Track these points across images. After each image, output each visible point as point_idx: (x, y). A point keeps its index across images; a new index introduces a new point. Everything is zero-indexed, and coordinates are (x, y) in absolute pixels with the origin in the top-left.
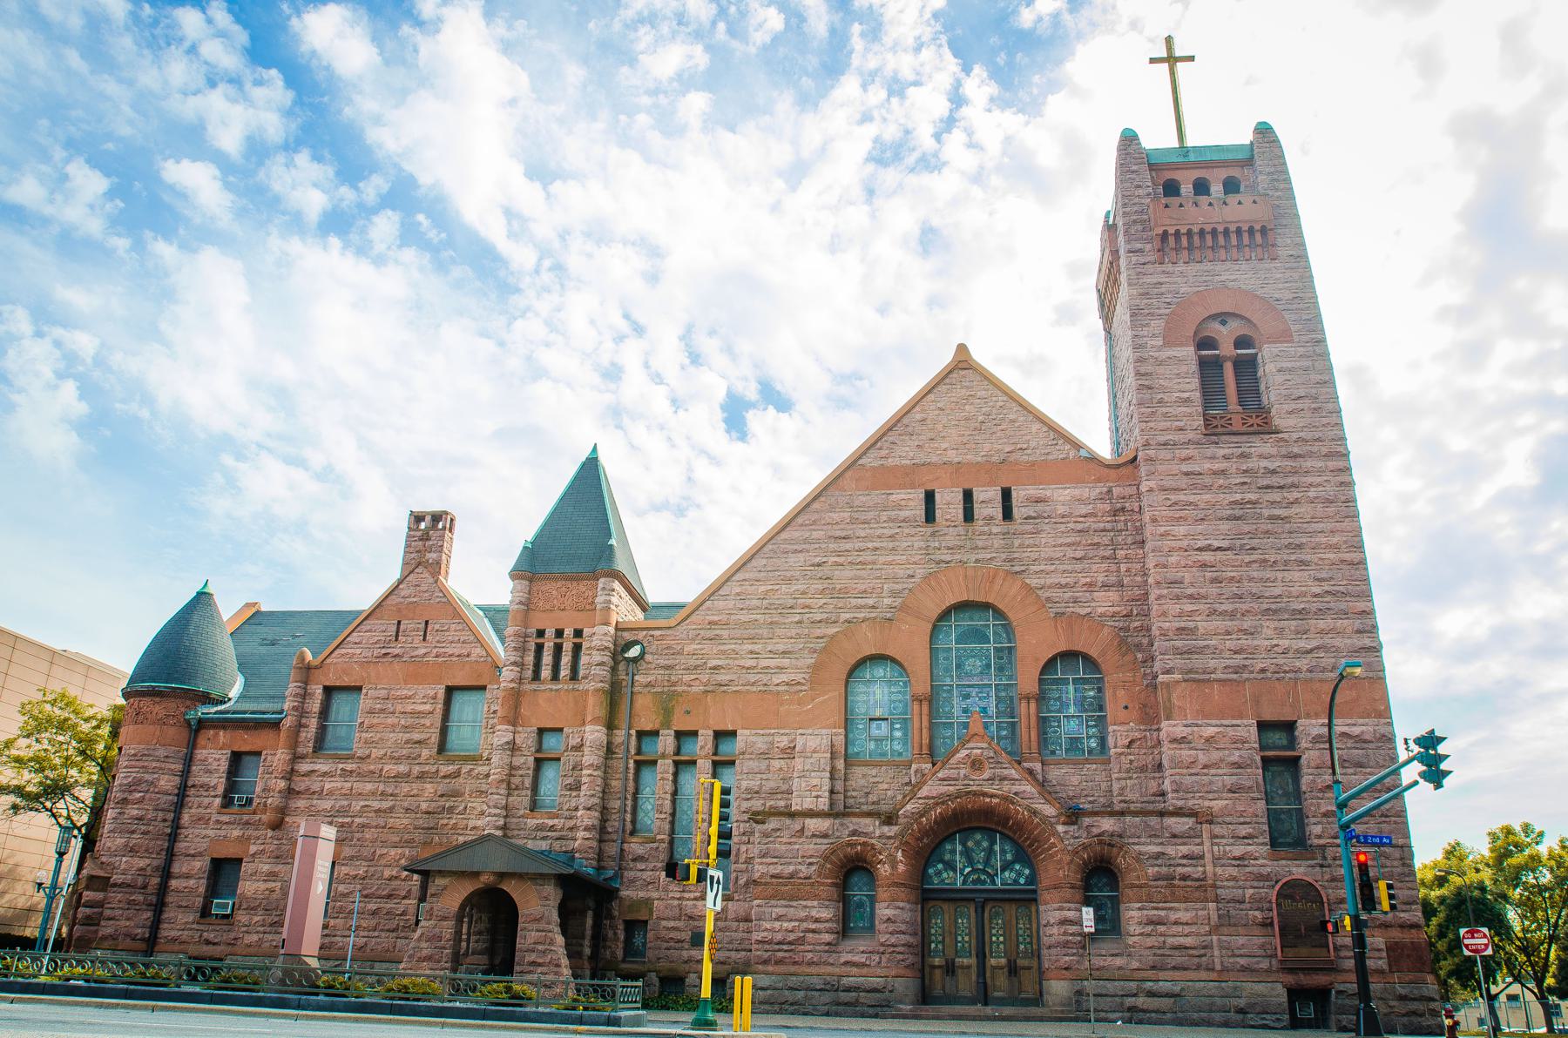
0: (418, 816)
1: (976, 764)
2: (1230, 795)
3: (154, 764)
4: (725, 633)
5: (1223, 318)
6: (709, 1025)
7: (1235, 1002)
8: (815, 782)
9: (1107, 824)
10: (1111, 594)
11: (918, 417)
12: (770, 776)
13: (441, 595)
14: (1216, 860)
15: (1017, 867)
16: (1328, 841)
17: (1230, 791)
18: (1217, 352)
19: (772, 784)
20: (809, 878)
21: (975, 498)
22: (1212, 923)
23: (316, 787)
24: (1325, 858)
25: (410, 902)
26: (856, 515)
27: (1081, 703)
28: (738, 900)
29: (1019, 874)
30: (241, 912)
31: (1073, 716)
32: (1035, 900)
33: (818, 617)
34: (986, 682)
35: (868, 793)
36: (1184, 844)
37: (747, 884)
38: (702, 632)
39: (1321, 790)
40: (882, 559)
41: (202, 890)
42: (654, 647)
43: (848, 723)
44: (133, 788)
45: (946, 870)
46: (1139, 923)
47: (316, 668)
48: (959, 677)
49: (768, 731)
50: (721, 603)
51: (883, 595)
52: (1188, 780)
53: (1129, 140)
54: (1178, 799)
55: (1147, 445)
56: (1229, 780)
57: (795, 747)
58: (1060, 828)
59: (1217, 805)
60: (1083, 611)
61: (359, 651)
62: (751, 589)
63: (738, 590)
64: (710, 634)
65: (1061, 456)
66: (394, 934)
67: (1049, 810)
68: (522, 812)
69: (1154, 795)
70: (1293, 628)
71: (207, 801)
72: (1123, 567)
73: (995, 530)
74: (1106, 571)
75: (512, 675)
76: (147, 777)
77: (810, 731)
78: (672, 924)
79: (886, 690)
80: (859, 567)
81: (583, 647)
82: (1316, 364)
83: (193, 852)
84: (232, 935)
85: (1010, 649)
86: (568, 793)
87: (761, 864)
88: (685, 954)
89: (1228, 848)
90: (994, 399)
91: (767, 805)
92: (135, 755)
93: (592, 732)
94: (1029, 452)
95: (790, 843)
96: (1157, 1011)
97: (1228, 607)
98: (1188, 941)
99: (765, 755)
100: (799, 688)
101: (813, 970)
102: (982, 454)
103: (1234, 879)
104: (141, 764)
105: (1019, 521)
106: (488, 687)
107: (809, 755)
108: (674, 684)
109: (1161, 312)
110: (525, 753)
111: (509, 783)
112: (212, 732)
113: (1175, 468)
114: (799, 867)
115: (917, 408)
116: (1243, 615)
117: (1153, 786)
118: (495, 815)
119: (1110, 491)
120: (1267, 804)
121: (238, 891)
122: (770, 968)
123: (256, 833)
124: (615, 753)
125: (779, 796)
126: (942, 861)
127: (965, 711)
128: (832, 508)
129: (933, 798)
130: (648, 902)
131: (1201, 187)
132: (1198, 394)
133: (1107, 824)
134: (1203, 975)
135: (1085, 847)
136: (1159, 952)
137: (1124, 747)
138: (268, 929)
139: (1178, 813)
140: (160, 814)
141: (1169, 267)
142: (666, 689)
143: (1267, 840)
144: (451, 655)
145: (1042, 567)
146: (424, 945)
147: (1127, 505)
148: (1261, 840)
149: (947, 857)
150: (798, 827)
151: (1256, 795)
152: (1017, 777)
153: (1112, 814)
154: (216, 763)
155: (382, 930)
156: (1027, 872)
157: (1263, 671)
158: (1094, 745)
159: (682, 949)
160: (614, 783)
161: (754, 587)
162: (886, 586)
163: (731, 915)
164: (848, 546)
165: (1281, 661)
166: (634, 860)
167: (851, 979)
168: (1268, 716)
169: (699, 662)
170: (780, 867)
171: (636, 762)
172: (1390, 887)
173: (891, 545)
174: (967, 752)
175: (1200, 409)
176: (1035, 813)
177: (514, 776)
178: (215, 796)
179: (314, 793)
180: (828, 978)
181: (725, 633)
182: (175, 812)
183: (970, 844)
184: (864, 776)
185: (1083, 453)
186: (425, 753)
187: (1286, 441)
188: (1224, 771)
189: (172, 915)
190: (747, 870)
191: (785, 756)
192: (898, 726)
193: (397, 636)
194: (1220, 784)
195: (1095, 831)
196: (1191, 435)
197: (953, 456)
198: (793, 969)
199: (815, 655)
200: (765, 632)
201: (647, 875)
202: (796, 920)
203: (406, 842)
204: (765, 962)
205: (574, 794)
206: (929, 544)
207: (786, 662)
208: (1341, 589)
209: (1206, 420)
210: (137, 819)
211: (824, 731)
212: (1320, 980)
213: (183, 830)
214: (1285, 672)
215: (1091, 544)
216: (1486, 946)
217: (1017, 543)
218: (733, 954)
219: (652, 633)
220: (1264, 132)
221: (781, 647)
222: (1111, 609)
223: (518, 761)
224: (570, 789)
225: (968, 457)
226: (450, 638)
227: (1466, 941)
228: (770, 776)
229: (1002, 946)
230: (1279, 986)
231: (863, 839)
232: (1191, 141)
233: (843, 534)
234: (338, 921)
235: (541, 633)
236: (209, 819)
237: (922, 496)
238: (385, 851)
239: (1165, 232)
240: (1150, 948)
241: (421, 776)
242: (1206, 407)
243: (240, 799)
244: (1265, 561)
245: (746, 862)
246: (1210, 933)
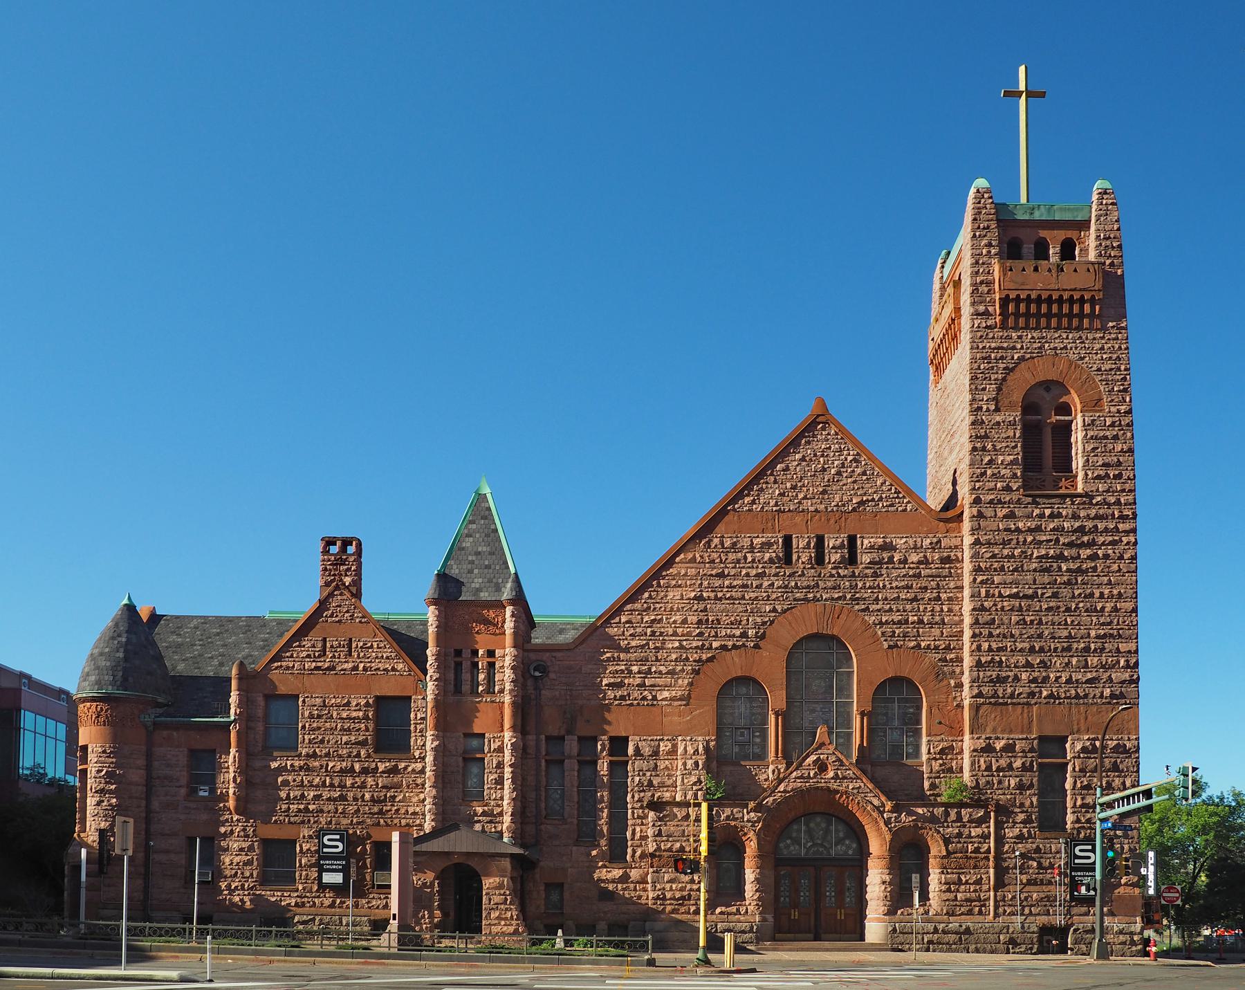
1: (822, 767)
15: (847, 842)
29: (849, 847)
45: (793, 844)
91: (656, 796)
126: (791, 838)
147: (952, 554)
149: (794, 835)
171: (546, 761)
183: (812, 825)
192: (758, 734)
216: (1178, 898)
219: (554, 654)
229: (833, 899)
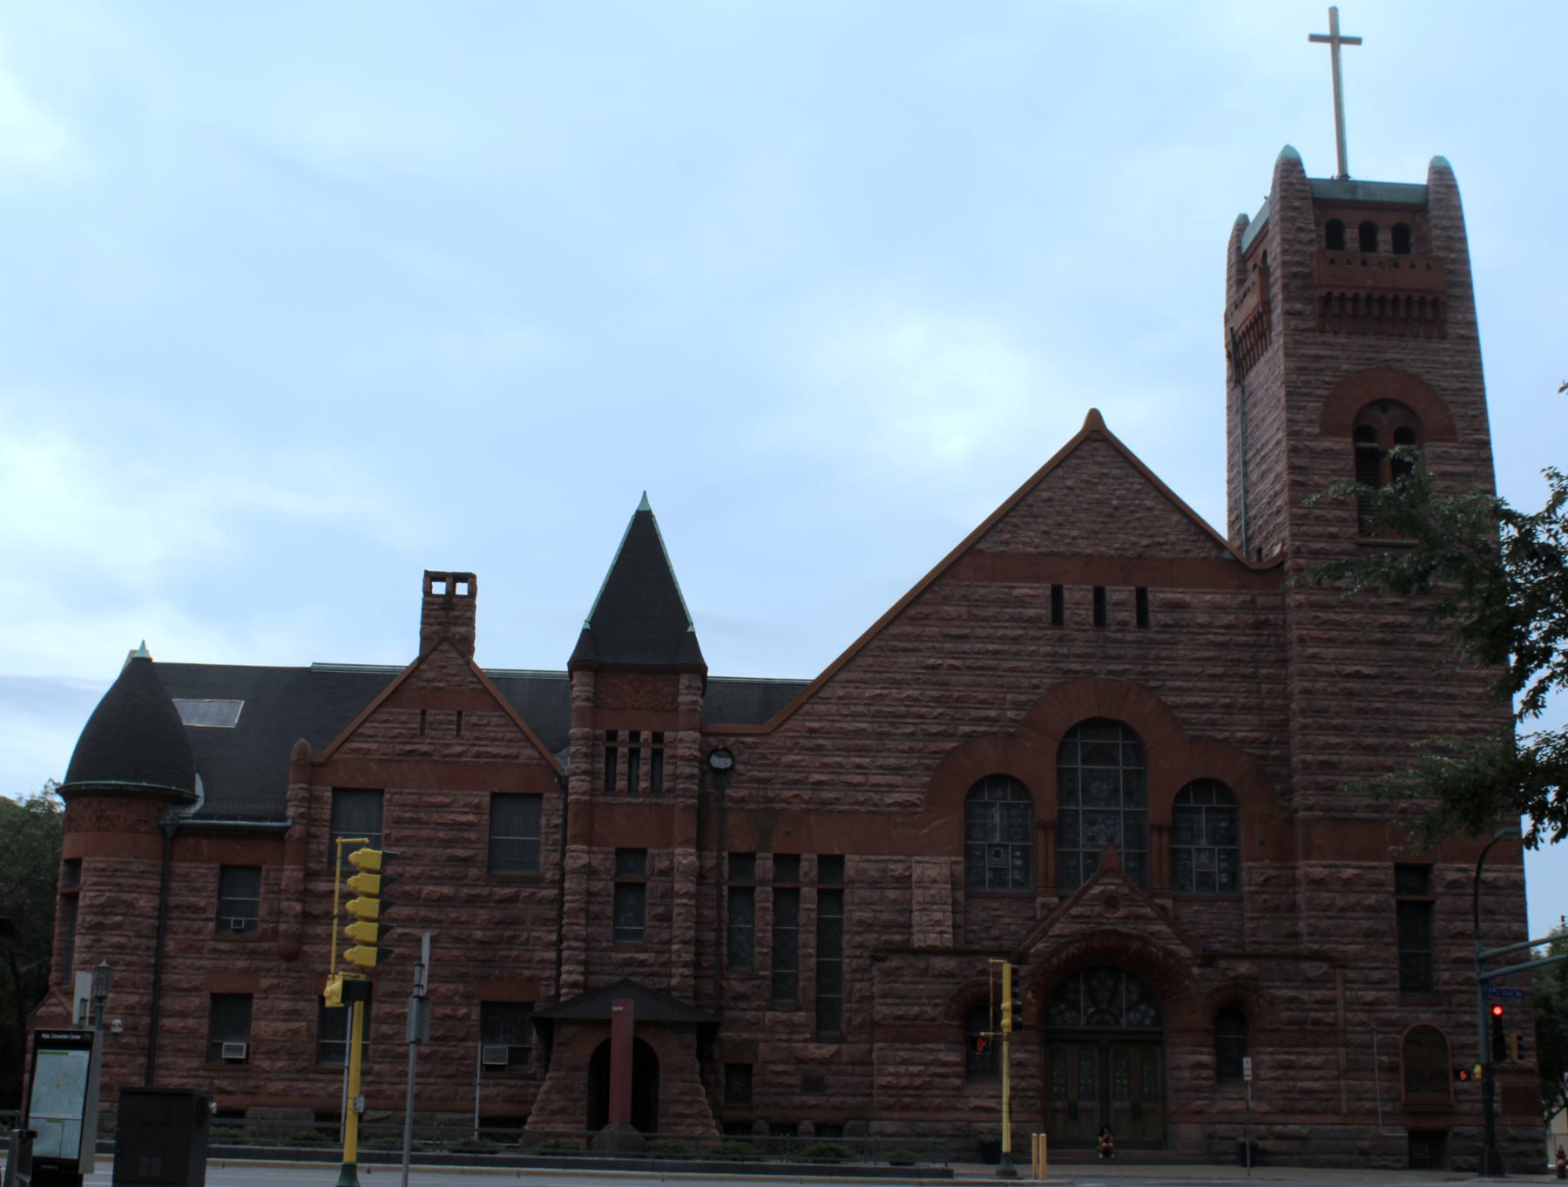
1: (1111, 901)
5: (1383, 404)
6: (1013, 1174)
8: (938, 916)
9: (1244, 968)
10: (1250, 717)
11: (1045, 495)
13: (475, 680)
15: (1143, 1007)
16: (1456, 987)
18: (1375, 445)
21: (1107, 599)
24: (1450, 1004)
26: (975, 611)
31: (1205, 849)
33: (934, 729)
34: (1113, 808)
36: (1318, 988)
41: (205, 1030)
42: (746, 756)
44: (108, 910)
46: (1271, 1068)
47: (321, 765)
48: (1085, 802)
51: (1007, 706)
52: (1325, 923)
53: (1289, 167)
55: (1297, 552)
58: (1196, 970)
60: (1220, 736)
62: (856, 692)
63: (841, 693)
64: (809, 743)
65: (1202, 555)
67: (1185, 951)
68: (604, 944)
69: (1287, 936)
71: (198, 925)
73: (1130, 637)
74: (1245, 692)
75: (585, 786)
77: (927, 859)
78: (780, 1068)
81: (665, 755)
82: (1479, 469)
85: (1140, 772)
86: (658, 924)
88: (797, 1100)
92: (103, 870)
94: (1167, 547)
97: (1371, 741)
98: (1316, 1085)
100: (913, 809)
101: (942, 1116)
102: (1117, 546)
103: (1362, 1023)
105: (1155, 629)
107: (928, 885)
110: (603, 877)
111: (587, 911)
112: (191, 841)
114: (925, 1008)
115: (1043, 485)
119: (1253, 601)
122: (895, 1115)
123: (266, 965)
128: (946, 600)
133: (1244, 968)
136: (1289, 1096)
137: (1258, 884)
138: (296, 1076)
139: (1314, 956)
141: (1330, 338)
142: (762, 806)
143: (1397, 986)
146: (555, 1097)
148: (1391, 986)
150: (922, 965)
151: (1388, 940)
155: (440, 1076)
156: (1152, 1012)
158: (1224, 880)
164: (966, 647)
167: (981, 1124)
170: (904, 1008)
172: (1519, 1038)
174: (1102, 888)
175: (1355, 514)
176: (1171, 954)
178: (207, 920)
180: (958, 1124)
185: (1226, 555)
186: (473, 872)
189: (170, 1059)
191: (900, 885)
192: (1018, 854)
193: (422, 729)
195: (1231, 974)
196: (1345, 545)
197: (1084, 547)
199: (931, 773)
201: (751, 1015)
202: (922, 1064)
205: (665, 925)
207: (897, 779)
211: (943, 859)
213: (169, 961)
219: (742, 739)
220: (1442, 174)
221: (892, 762)
223: (598, 886)
229: (1125, 1089)
234: (383, 1066)
235: (612, 735)
237: (1048, 592)
244: (1412, 692)
246: (1337, 1078)
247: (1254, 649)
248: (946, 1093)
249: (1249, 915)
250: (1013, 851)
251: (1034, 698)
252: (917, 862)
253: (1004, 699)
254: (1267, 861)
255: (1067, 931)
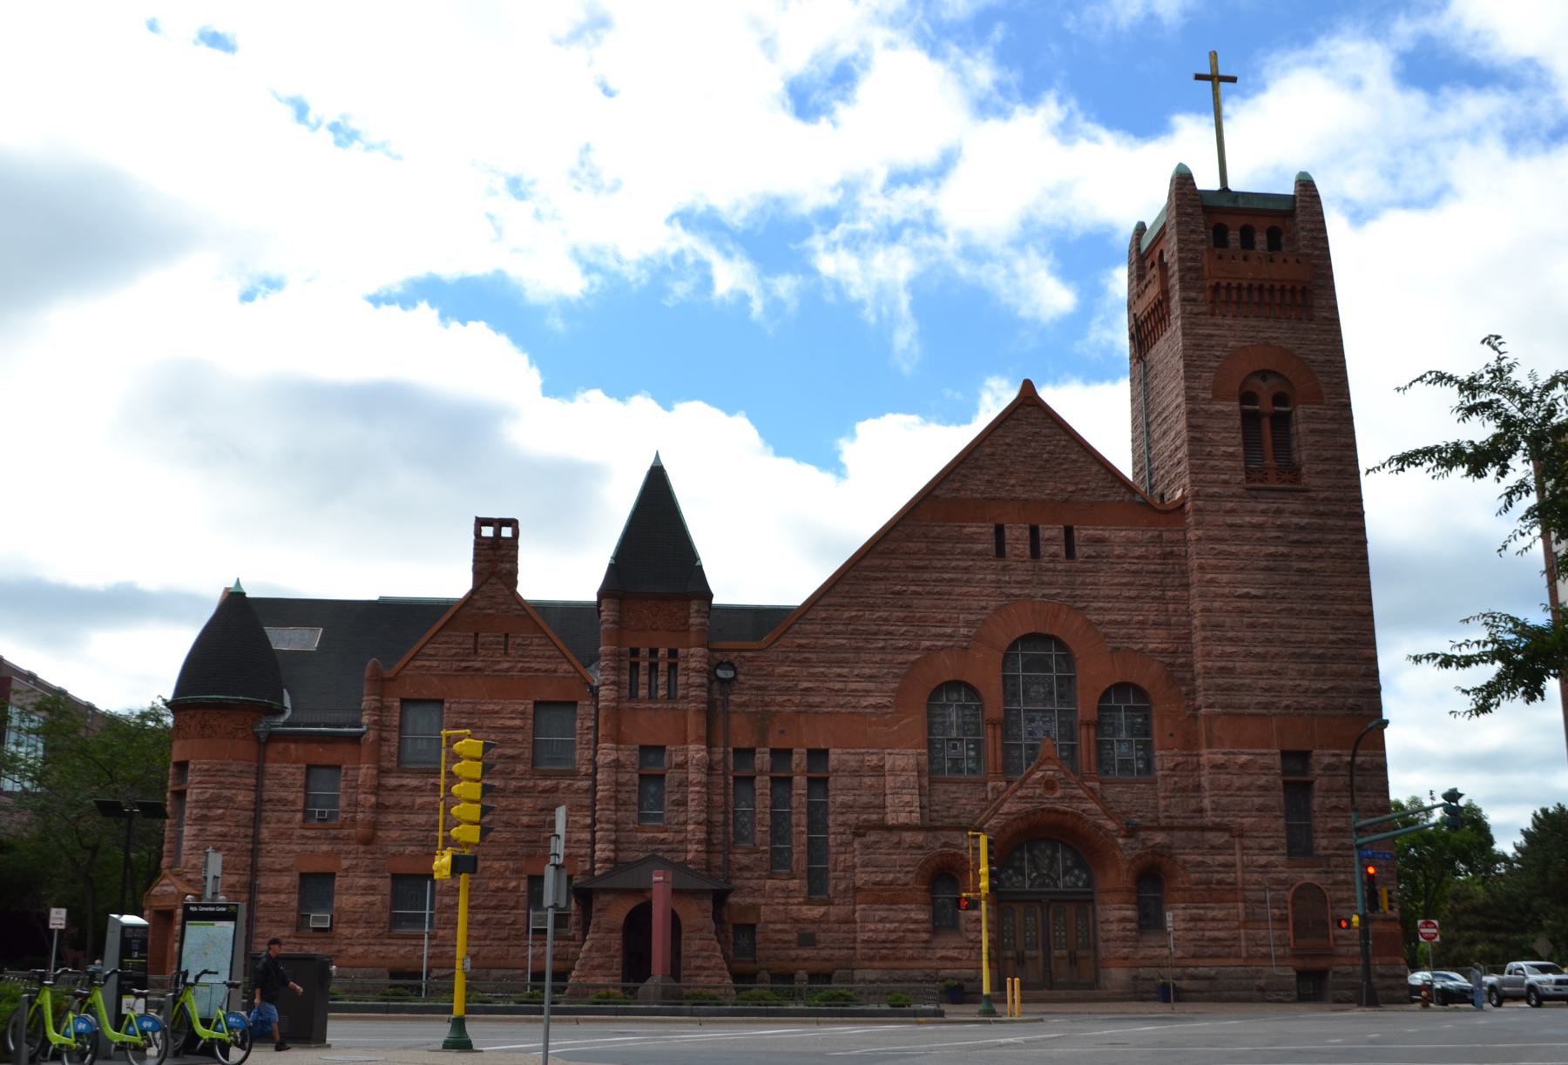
0: (519, 829)
1: (1050, 785)
2: (1258, 813)
3: (231, 780)
4: (813, 656)
5: (1264, 374)
7: (1257, 982)
8: (907, 798)
9: (1160, 838)
10: (1160, 631)
11: (988, 450)
12: (862, 792)
13: (519, 607)
14: (1245, 866)
17: (1258, 810)
18: (1257, 407)
19: (865, 799)
20: (906, 884)
22: (1241, 919)
23: (407, 801)
24: (1329, 866)
25: (520, 911)
27: (1132, 730)
28: (839, 904)
30: (340, 925)
32: (1092, 901)
35: (949, 808)
36: (1220, 854)
37: (846, 890)
38: (791, 654)
39: (1329, 810)
40: (958, 590)
41: (295, 904)
42: (746, 668)
43: (930, 744)
44: (212, 804)
46: (1183, 920)
49: (859, 750)
50: (808, 627)
52: (1225, 801)
54: (1217, 816)
56: (1258, 801)
57: (884, 765)
58: (1120, 841)
59: (1248, 821)
61: (435, 664)
63: (824, 615)
64: (798, 657)
66: (506, 943)
68: (631, 826)
69: (1194, 811)
70: (1312, 670)
71: (286, 816)
72: (1171, 607)
73: (1060, 567)
75: (613, 695)
76: (226, 793)
77: (896, 751)
78: (779, 926)
79: (960, 713)
80: (936, 597)
83: (279, 867)
84: (336, 948)
87: (863, 872)
88: (793, 953)
89: (1255, 858)
90: (1058, 438)
93: (698, 751)
94: (1089, 492)
95: (889, 854)
96: (1198, 991)
98: (1221, 934)
99: (855, 773)
100: (885, 710)
101: (914, 964)
104: (217, 779)
105: (1081, 559)
106: (580, 702)
108: (767, 704)
109: (1211, 364)
112: (281, 745)
113: (1220, 519)
114: (898, 875)
115: (987, 443)
116: (1273, 658)
117: (1193, 804)
118: (607, 830)
119: (1160, 536)
120: (1287, 820)
121: (335, 905)
122: (876, 964)
123: (345, 848)
124: (715, 770)
125: (872, 810)
127: (1031, 733)
129: (1013, 814)
130: (755, 908)
131: (1247, 236)
132: (1241, 449)
133: (1160, 838)
134: (1232, 961)
135: (1139, 857)
136: (1199, 943)
138: (372, 941)
139: (1217, 828)
140: (242, 830)
141: (1219, 320)
142: (760, 709)
143: (1285, 851)
144: (537, 670)
145: (1100, 604)
146: (594, 954)
148: (1281, 851)
150: (895, 839)
151: (1278, 814)
152: (1085, 795)
153: (1163, 829)
154: (290, 778)
155: (493, 939)
156: (1084, 876)
157: (1287, 707)
158: (1141, 766)
159: (790, 948)
160: (716, 798)
161: (839, 613)
162: (961, 617)
163: (832, 918)
164: (926, 576)
165: (1302, 700)
166: (740, 869)
168: (1290, 746)
169: (790, 684)
171: (735, 778)
173: (965, 577)
175: (1242, 464)
176: (1100, 827)
177: (620, 792)
179: (405, 807)
181: (813, 656)
182: (254, 827)
184: (945, 792)
186: (520, 768)
187: (1314, 500)
188: (1254, 793)
190: (845, 878)
192: (972, 746)
194: (1250, 804)
195: (1150, 843)
198: (896, 964)
199: (898, 680)
200: (851, 656)
201: (753, 883)
202: (897, 922)
203: (509, 854)
204: (872, 959)
205: (681, 809)
206: (999, 577)
207: (871, 686)
208: (1353, 637)
209: (1247, 473)
210: (220, 836)
211: (910, 751)
212: (1321, 964)
213: (263, 846)
214: (1305, 709)
215: (1143, 585)
217: (1079, 580)
218: (837, 953)
220: (1306, 185)
222: (1160, 646)
223: (624, 777)
224: (677, 805)
225: (1035, 494)
226: (534, 653)
227: (1422, 931)
228: (862, 792)
230: (1290, 969)
231: (953, 851)
232: (1234, 185)
233: (921, 563)
234: (446, 931)
236: (292, 834)
238: (488, 863)
239: (1218, 284)
240: (1192, 940)
241: (518, 791)
242: (1247, 461)
243: (321, 813)
244: (1292, 609)
245: (844, 870)
247: (1161, 576)
248: (917, 945)
249: (1163, 794)
250: (967, 744)
251: (983, 617)
252: (890, 754)
253: (958, 618)
254: (1176, 750)
255: (1014, 810)
